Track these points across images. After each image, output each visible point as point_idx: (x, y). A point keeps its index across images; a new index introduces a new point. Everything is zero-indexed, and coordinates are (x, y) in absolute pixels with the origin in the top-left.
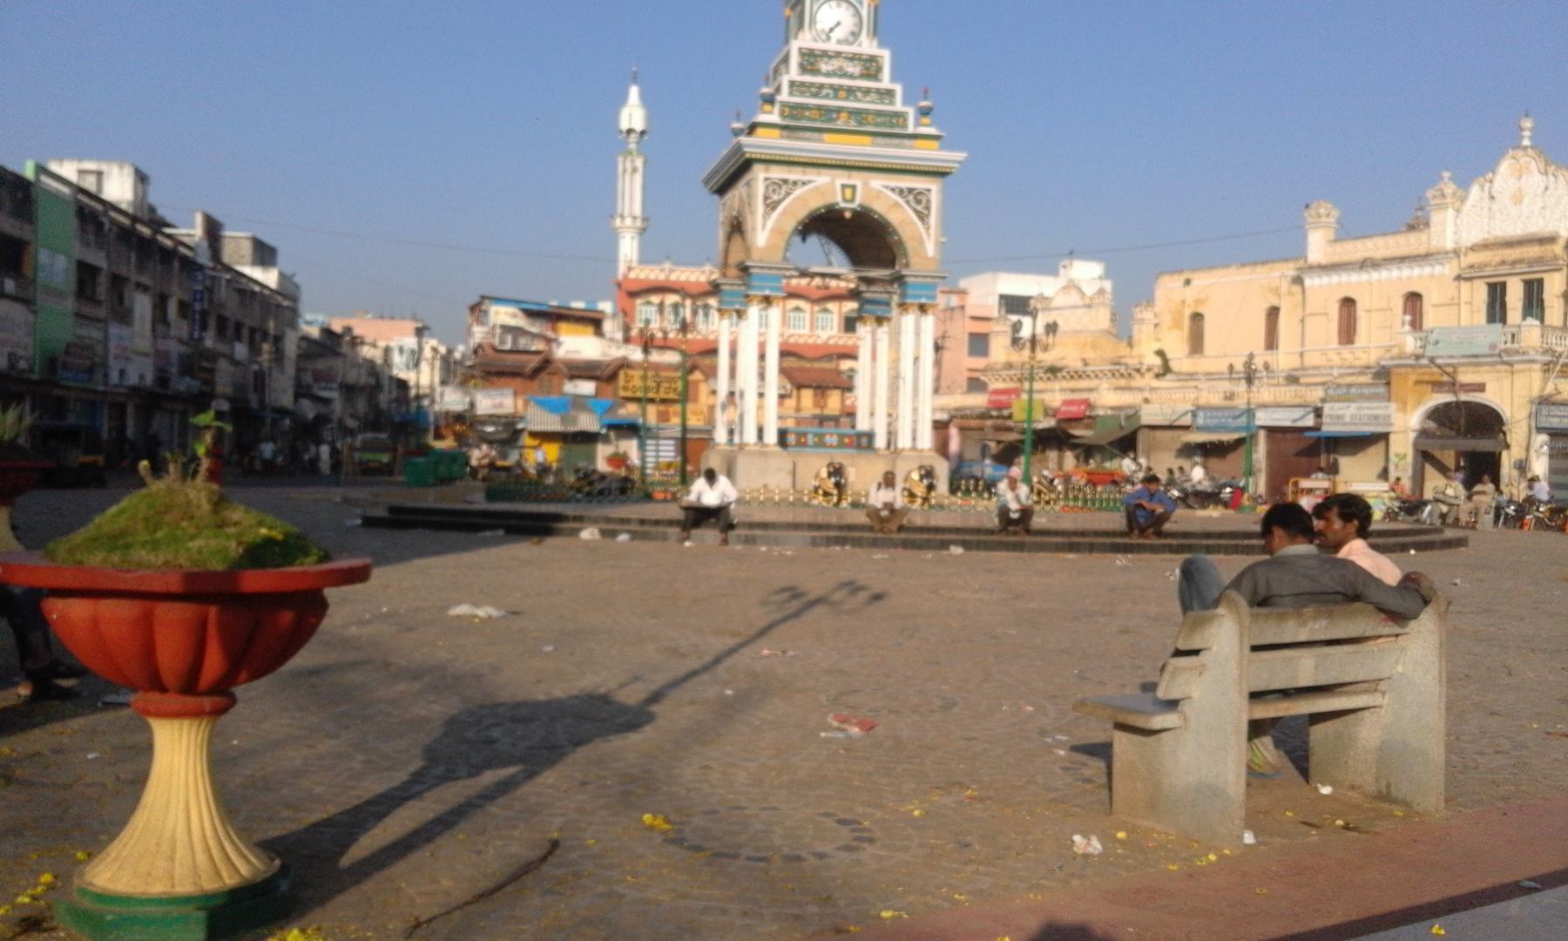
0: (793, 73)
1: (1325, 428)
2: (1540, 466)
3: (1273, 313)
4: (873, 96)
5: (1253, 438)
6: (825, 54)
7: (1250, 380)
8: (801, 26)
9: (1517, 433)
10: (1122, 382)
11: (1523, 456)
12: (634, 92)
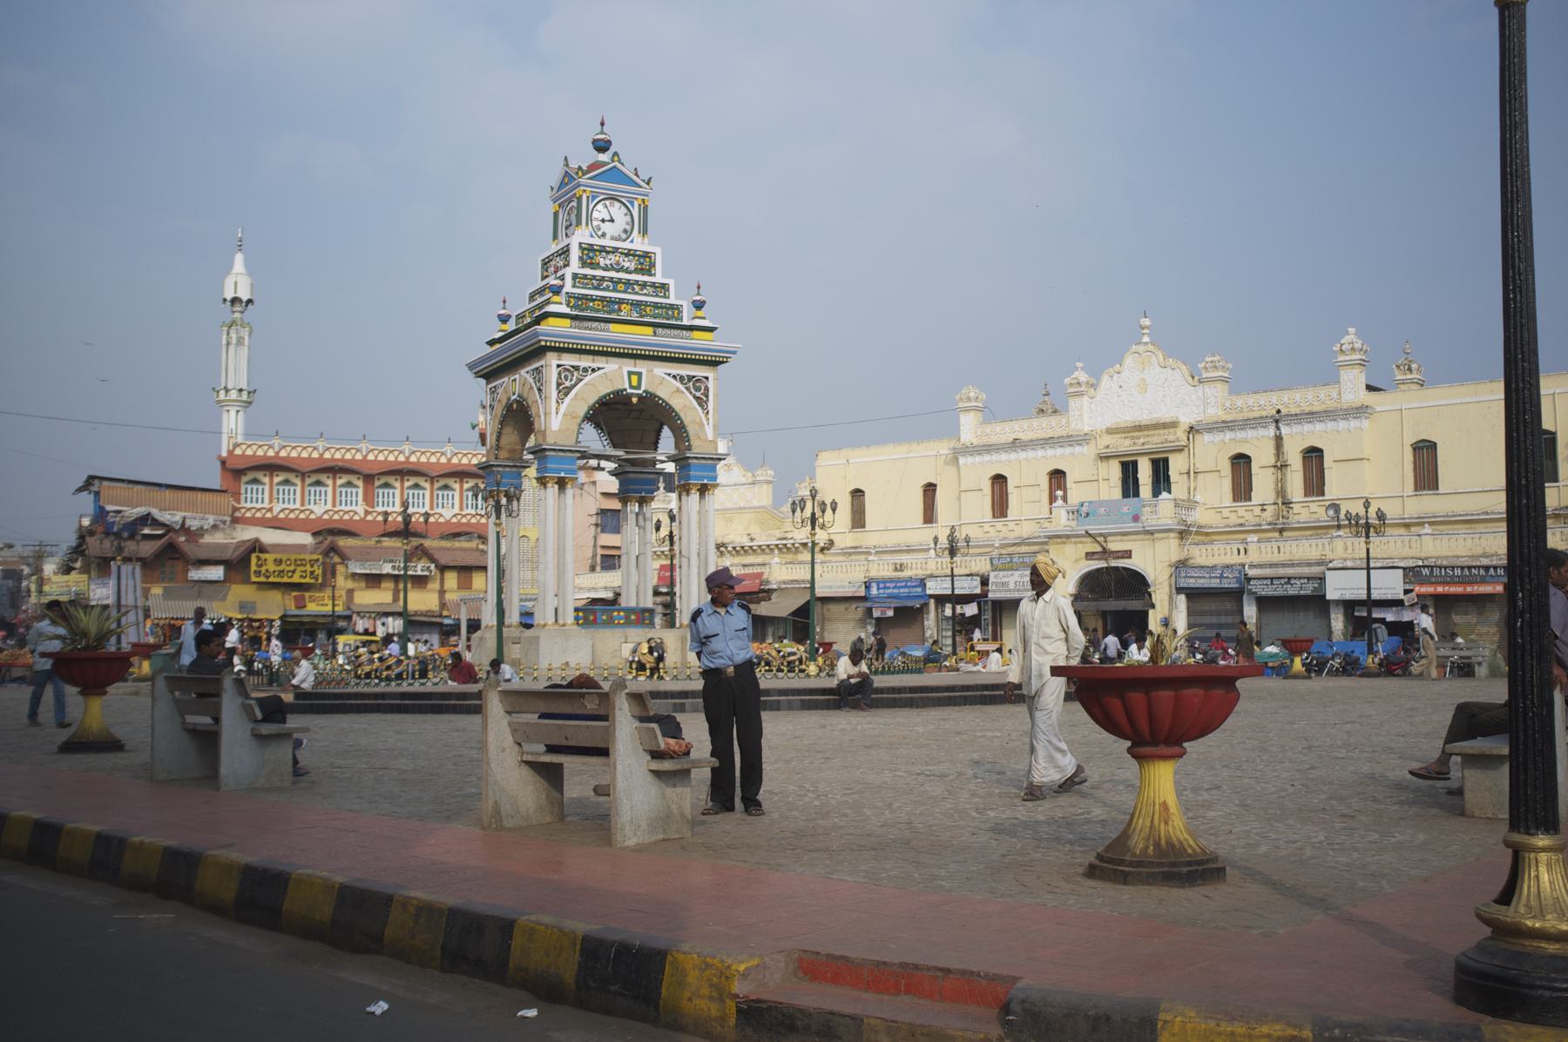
0: (574, 266)
1: (991, 595)
2: (1181, 623)
3: (930, 489)
4: (621, 287)
5: (926, 605)
6: (603, 249)
7: (953, 552)
8: (579, 223)
9: (1160, 593)
10: (790, 557)
11: (1166, 613)
12: (239, 258)
